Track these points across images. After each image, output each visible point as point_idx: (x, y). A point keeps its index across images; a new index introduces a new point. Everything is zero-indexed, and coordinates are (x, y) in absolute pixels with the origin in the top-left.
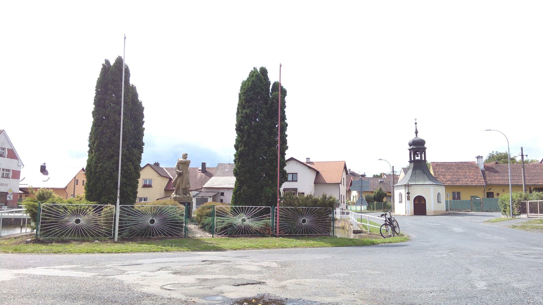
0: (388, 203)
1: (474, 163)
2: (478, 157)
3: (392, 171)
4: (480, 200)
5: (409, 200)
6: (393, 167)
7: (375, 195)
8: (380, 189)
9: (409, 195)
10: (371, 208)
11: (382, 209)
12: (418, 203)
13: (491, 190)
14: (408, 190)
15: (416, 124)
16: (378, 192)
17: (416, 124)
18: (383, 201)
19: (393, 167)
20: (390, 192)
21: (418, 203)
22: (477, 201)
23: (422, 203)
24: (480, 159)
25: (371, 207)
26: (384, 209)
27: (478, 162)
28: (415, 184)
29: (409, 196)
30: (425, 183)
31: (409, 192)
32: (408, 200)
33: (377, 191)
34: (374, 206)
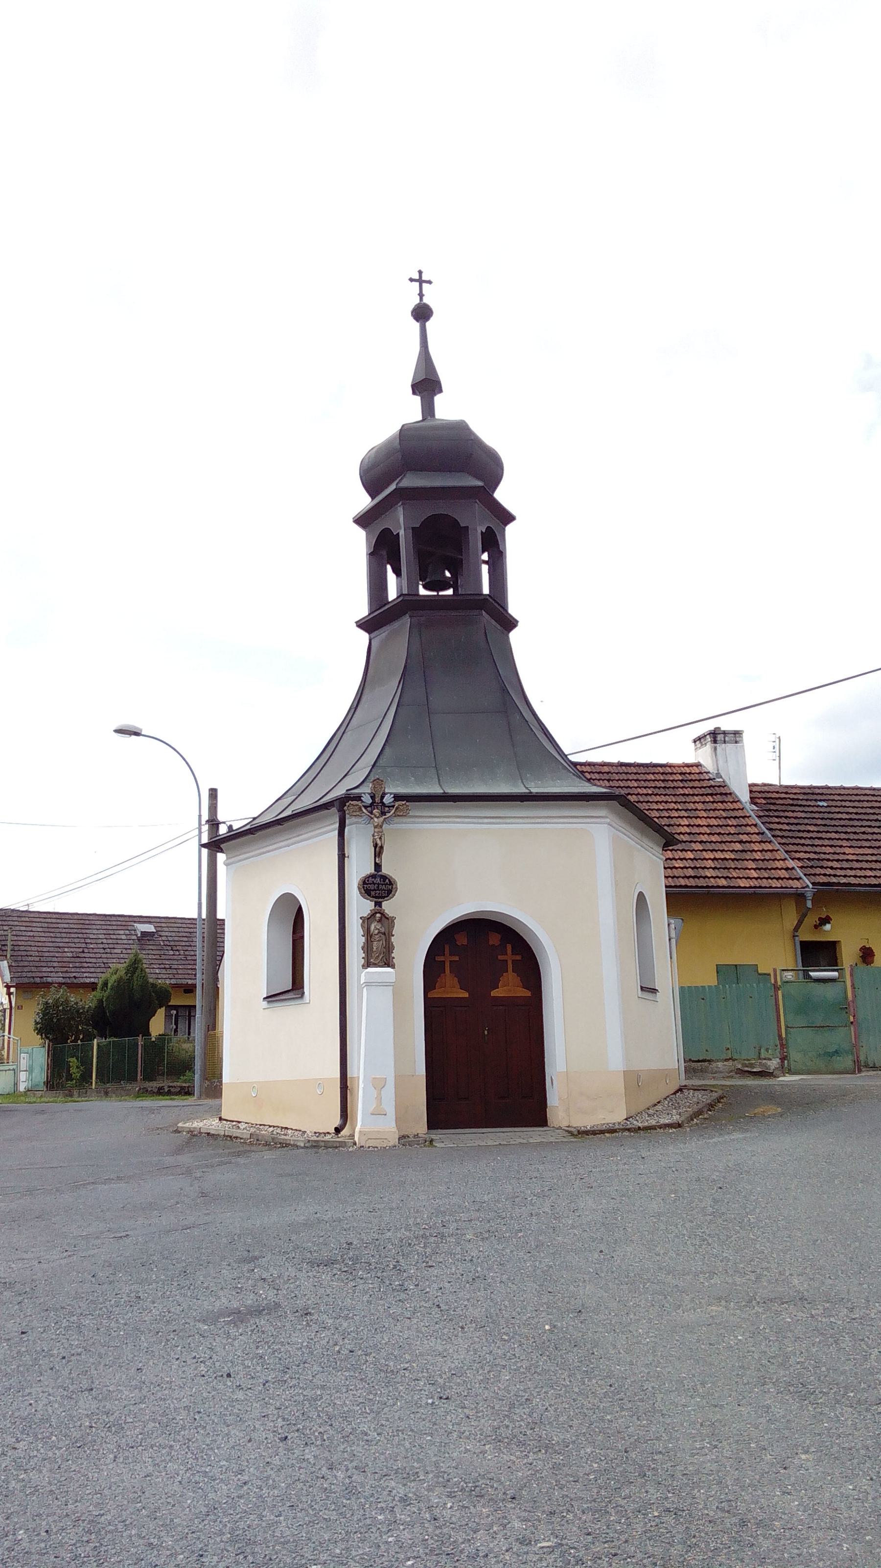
0: (179, 1045)
1: (697, 770)
2: (720, 737)
3: (205, 817)
4: (838, 986)
5: (388, 962)
6: (213, 794)
7: (100, 1001)
8: (135, 966)
9: (388, 906)
10: (70, 1077)
11: (132, 1078)
12: (466, 995)
13: (828, 927)
14: (378, 851)
15: (422, 313)
16: (120, 980)
17: (422, 313)
18: (147, 1033)
19: (213, 794)
20: (190, 990)
21: (466, 995)
22: (820, 988)
23: (494, 993)
24: (730, 747)
25: (73, 1070)
26: (148, 1077)
27: (721, 763)
28: (437, 790)
29: (387, 921)
30: (536, 789)
31: (385, 871)
32: (368, 964)
33: (115, 977)
34: (86, 1062)
